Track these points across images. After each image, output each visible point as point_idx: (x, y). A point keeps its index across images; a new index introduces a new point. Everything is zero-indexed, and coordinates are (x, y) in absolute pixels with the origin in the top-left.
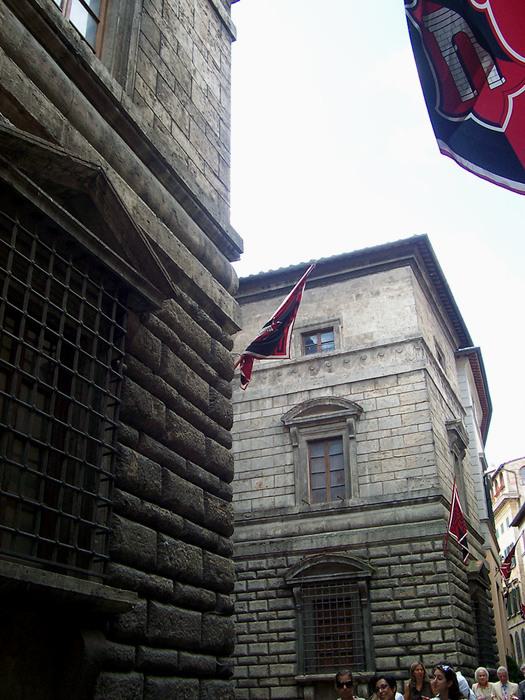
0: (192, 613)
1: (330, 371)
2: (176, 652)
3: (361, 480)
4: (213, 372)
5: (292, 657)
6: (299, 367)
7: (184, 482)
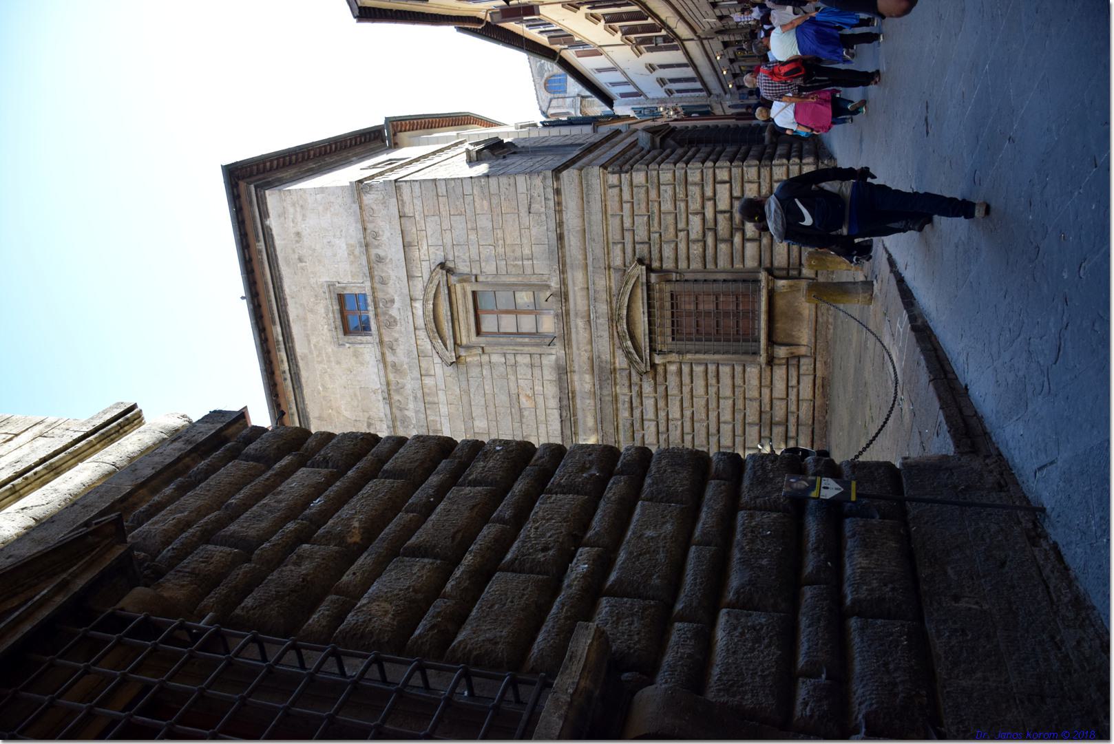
0: (636, 517)
1: (393, 301)
2: (693, 548)
3: (529, 271)
4: (286, 460)
5: (738, 369)
6: (386, 339)
7: (429, 524)
